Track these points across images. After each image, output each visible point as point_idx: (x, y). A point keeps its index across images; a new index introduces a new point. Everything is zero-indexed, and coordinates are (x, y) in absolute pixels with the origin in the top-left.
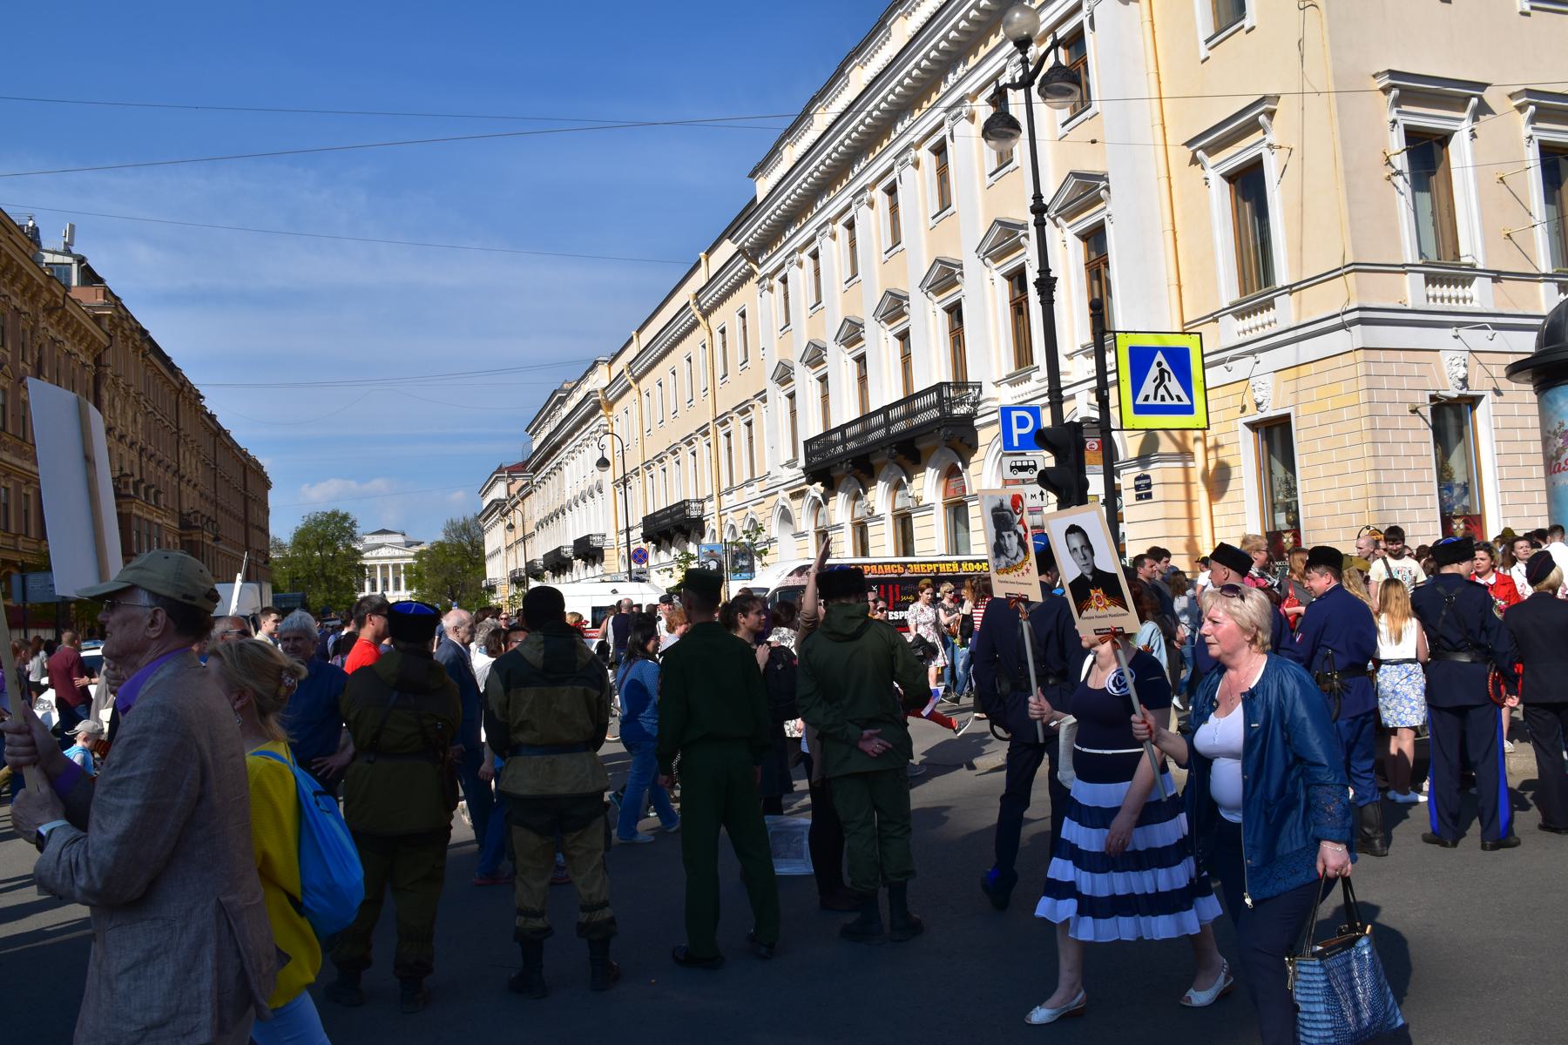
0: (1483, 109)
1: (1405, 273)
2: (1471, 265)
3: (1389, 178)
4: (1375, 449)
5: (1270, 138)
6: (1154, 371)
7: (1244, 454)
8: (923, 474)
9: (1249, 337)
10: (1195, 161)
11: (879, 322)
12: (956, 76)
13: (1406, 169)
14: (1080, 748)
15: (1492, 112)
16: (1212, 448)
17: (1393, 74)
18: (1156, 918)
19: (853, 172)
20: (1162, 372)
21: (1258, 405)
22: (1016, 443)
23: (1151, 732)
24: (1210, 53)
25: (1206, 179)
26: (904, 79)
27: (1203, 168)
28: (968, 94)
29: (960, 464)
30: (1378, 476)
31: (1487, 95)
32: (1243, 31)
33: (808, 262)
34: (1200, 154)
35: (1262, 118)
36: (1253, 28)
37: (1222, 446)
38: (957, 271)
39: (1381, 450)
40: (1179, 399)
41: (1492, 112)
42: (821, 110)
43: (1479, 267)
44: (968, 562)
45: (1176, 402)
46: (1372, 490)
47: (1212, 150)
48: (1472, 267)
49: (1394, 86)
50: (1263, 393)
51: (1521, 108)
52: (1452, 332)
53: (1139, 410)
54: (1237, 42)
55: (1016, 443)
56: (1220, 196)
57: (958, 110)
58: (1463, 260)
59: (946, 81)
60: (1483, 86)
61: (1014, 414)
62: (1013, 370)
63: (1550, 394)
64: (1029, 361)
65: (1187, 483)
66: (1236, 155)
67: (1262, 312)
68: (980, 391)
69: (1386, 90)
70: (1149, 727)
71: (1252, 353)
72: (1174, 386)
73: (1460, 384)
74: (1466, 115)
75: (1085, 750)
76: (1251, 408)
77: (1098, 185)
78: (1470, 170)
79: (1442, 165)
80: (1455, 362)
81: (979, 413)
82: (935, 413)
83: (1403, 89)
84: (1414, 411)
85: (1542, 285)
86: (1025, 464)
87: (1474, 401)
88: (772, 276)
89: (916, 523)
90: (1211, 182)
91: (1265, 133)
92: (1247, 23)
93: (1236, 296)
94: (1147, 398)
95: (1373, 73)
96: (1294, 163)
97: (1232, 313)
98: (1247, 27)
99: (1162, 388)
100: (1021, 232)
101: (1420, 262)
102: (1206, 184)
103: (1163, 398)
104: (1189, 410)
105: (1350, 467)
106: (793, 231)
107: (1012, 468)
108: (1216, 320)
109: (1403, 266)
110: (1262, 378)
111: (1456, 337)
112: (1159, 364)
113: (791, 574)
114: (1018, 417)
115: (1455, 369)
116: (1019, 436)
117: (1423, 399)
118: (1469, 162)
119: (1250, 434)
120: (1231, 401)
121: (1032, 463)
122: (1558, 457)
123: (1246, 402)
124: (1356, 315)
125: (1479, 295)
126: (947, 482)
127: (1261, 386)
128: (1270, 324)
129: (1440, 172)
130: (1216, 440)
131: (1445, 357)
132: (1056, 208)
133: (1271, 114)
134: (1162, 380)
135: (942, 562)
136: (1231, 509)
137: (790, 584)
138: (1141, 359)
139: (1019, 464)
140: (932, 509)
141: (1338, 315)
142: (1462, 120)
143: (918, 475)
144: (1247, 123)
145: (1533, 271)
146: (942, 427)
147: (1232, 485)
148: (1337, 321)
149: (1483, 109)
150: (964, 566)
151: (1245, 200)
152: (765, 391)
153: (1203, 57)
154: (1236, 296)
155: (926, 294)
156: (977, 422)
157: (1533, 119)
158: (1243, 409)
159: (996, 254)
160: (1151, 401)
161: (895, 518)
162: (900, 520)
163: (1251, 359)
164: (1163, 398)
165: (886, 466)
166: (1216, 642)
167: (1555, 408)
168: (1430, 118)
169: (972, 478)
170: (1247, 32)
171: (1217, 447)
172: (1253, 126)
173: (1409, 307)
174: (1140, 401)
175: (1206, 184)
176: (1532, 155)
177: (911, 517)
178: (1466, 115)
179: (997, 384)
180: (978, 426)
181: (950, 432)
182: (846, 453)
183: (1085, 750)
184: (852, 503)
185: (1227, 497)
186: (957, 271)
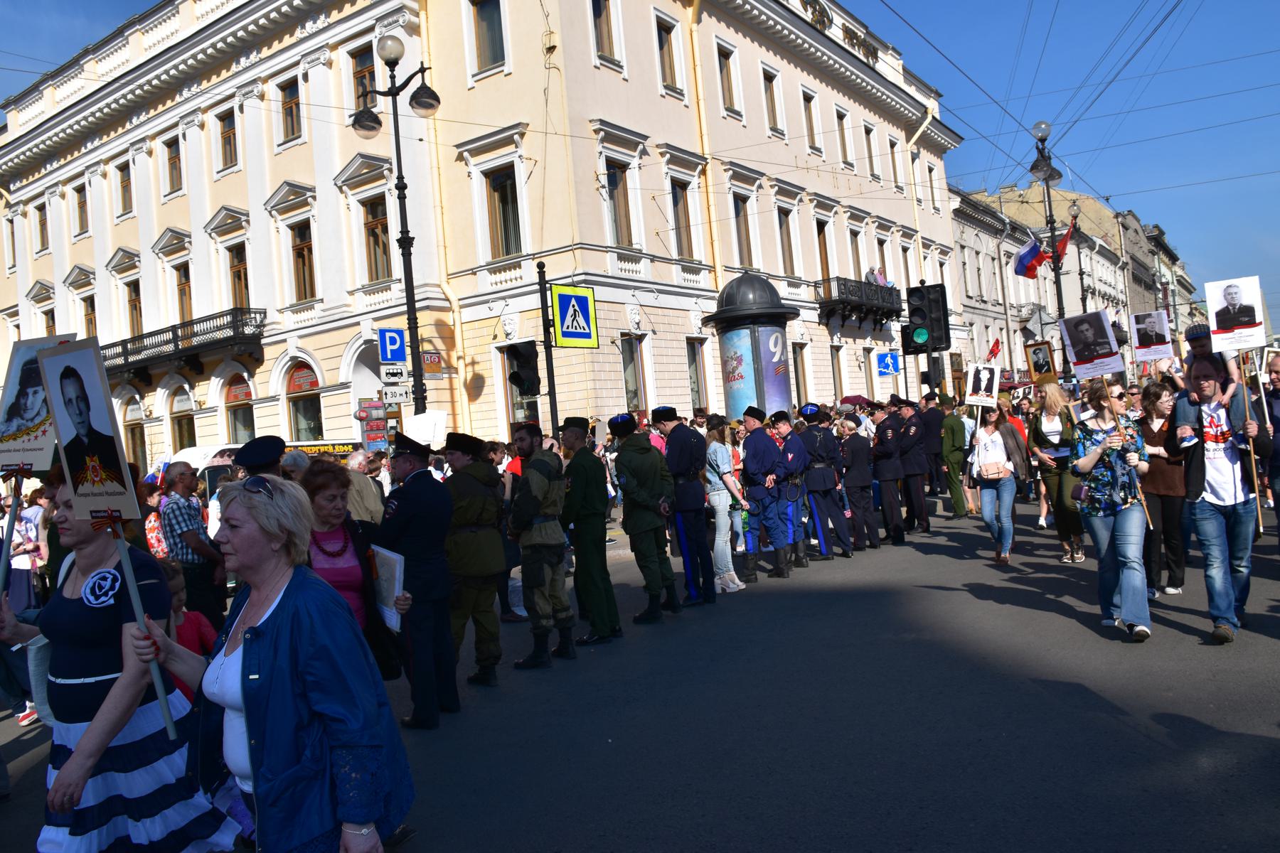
0: (644, 152)
1: (607, 252)
2: (640, 250)
3: (598, 189)
4: (594, 367)
5: (520, 151)
6: (571, 311)
7: (496, 371)
8: (207, 382)
9: (500, 287)
10: (460, 158)
11: (157, 254)
12: (248, 61)
13: (607, 185)
14: (52, 679)
15: (649, 155)
16: (469, 364)
17: (602, 122)
18: (170, 830)
19: (131, 122)
20: (575, 311)
21: (507, 335)
22: (389, 356)
23: (158, 649)
24: (475, 84)
25: (470, 173)
26: (199, 53)
27: (466, 164)
28: (260, 77)
29: (246, 375)
30: (595, 384)
31: (647, 143)
32: (502, 74)
33: (72, 197)
34: (466, 154)
35: (516, 137)
36: (510, 74)
37: (478, 363)
38: (244, 218)
39: (597, 367)
40: (584, 329)
41: (649, 155)
42: (92, 62)
43: (644, 252)
44: (340, 445)
45: (582, 331)
46: (592, 394)
47: (476, 152)
48: (640, 251)
49: (601, 130)
50: (511, 326)
51: (662, 154)
52: (631, 292)
53: (565, 334)
54: (495, 82)
55: (389, 356)
56: (479, 189)
57: (250, 88)
58: (635, 246)
59: (238, 62)
60: (646, 138)
61: (388, 335)
62: (294, 301)
63: (729, 335)
64: (304, 297)
65: (452, 389)
66: (495, 159)
67: (500, 273)
68: (265, 317)
69: (596, 131)
70: (155, 643)
71: (504, 298)
72: (581, 319)
73: (636, 326)
74: (636, 154)
75: (59, 681)
76: (501, 336)
77: (383, 167)
78: (639, 191)
79: (621, 184)
80: (633, 312)
81: (265, 334)
82: (229, 333)
83: (779, 187)
84: (613, 342)
85: (675, 266)
86: (395, 371)
87: (641, 338)
88: (26, 202)
89: (197, 423)
90: (473, 175)
91: (517, 147)
92: (506, 69)
93: (489, 259)
94: (568, 328)
95: (591, 119)
96: (538, 171)
97: (488, 269)
98: (506, 72)
99: (575, 321)
100: (309, 194)
101: (615, 246)
102: (469, 176)
103: (576, 329)
104: (588, 336)
105: (576, 378)
106: (55, 165)
107: (387, 374)
108: (475, 274)
109: (606, 247)
110: (511, 316)
111: (633, 296)
112: (573, 306)
113: (215, 456)
114: (390, 337)
115: (634, 316)
116: (391, 350)
117: (617, 334)
118: (639, 187)
119: (499, 355)
120: (485, 332)
121: (399, 371)
122: (733, 372)
123: (497, 332)
124: (582, 277)
125: (644, 270)
126: (229, 390)
127: (510, 321)
128: (516, 279)
129: (620, 186)
130: (473, 358)
131: (628, 308)
132: (343, 179)
133: (522, 135)
134: (575, 317)
135: (322, 445)
136: (485, 407)
137: (216, 464)
138: (564, 301)
139: (391, 371)
140: (216, 411)
141: (570, 277)
142: (634, 157)
143: (201, 383)
144: (507, 137)
145: (669, 257)
146: (237, 344)
147: (486, 390)
148: (569, 280)
149: (644, 152)
150: (336, 447)
151: (495, 191)
152: (17, 306)
153: (470, 86)
154: (489, 259)
155: (210, 234)
156: (263, 341)
157: (669, 162)
158: (495, 337)
159: (282, 208)
160: (570, 330)
161: (173, 419)
162: (176, 422)
163: (502, 303)
164: (576, 329)
165: (167, 376)
166: (232, 552)
167: (732, 343)
168: (619, 154)
169: (258, 386)
170: (506, 76)
171: (473, 363)
172: (509, 141)
173: (610, 275)
174: (565, 329)
175: (469, 176)
176: (668, 186)
177: (193, 418)
178: (636, 154)
179: (280, 311)
180: (265, 344)
181: (243, 348)
182: (127, 364)
183: (59, 681)
184: (124, 407)
185: (481, 399)
186: (244, 218)
